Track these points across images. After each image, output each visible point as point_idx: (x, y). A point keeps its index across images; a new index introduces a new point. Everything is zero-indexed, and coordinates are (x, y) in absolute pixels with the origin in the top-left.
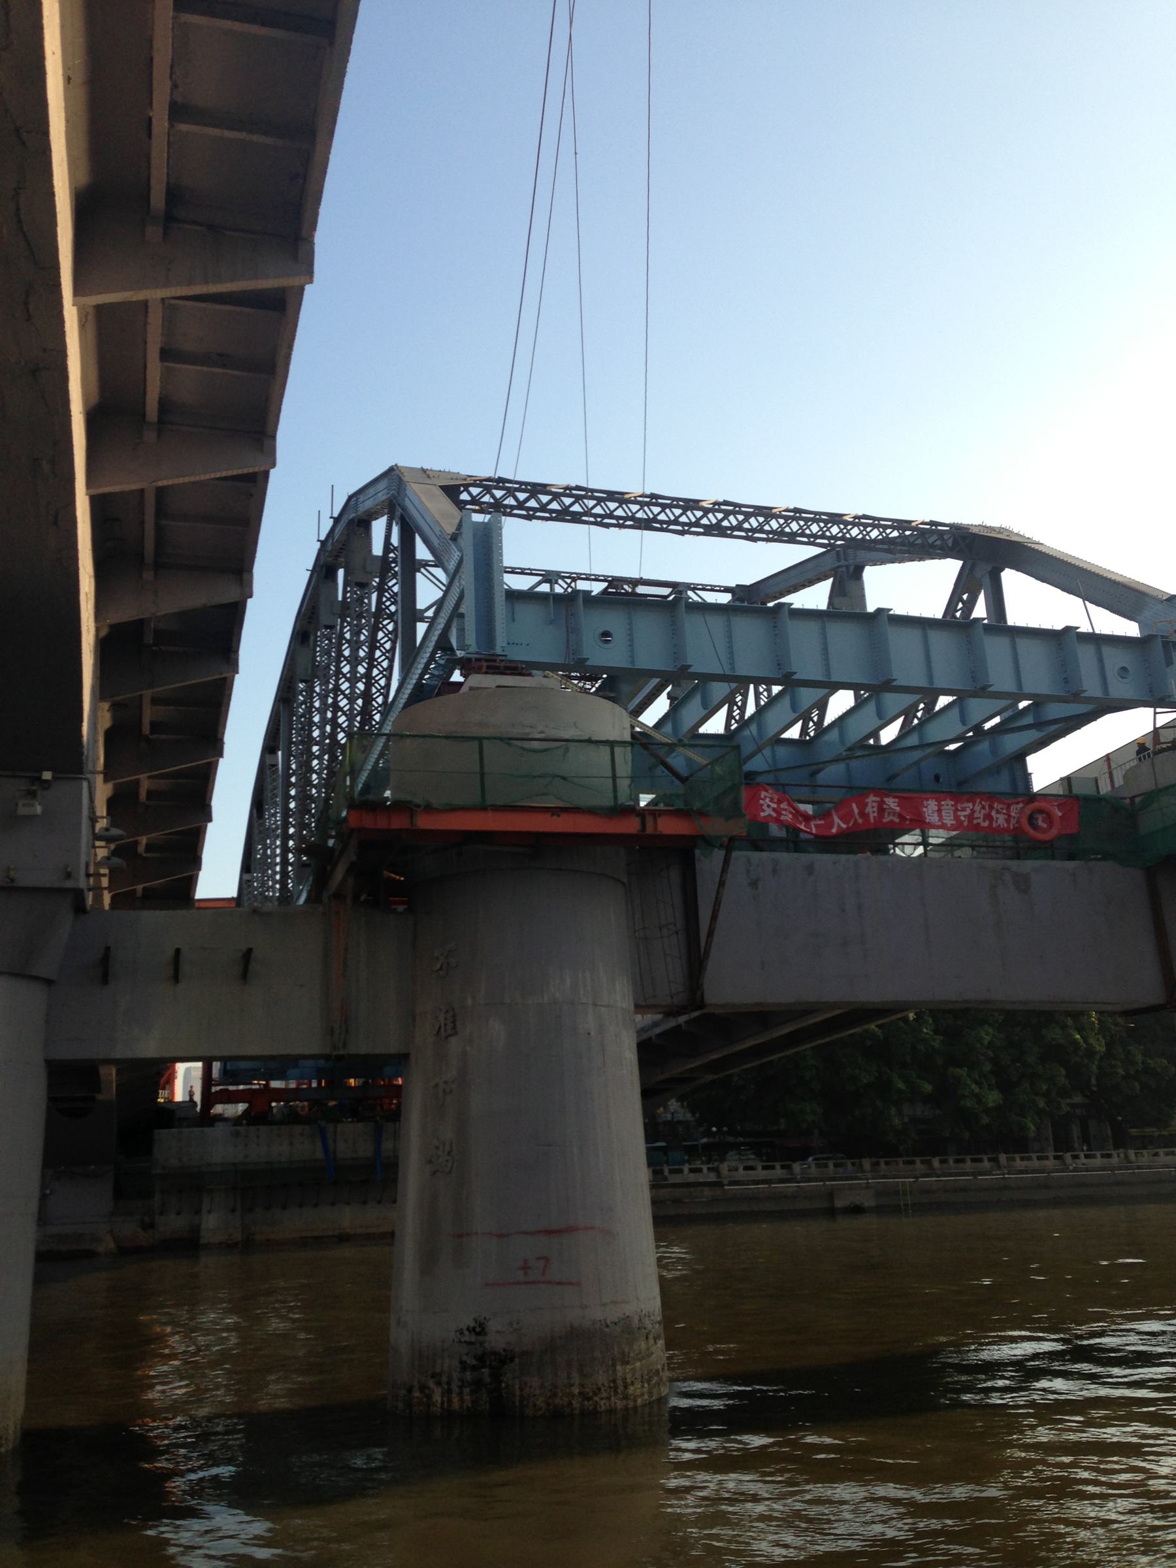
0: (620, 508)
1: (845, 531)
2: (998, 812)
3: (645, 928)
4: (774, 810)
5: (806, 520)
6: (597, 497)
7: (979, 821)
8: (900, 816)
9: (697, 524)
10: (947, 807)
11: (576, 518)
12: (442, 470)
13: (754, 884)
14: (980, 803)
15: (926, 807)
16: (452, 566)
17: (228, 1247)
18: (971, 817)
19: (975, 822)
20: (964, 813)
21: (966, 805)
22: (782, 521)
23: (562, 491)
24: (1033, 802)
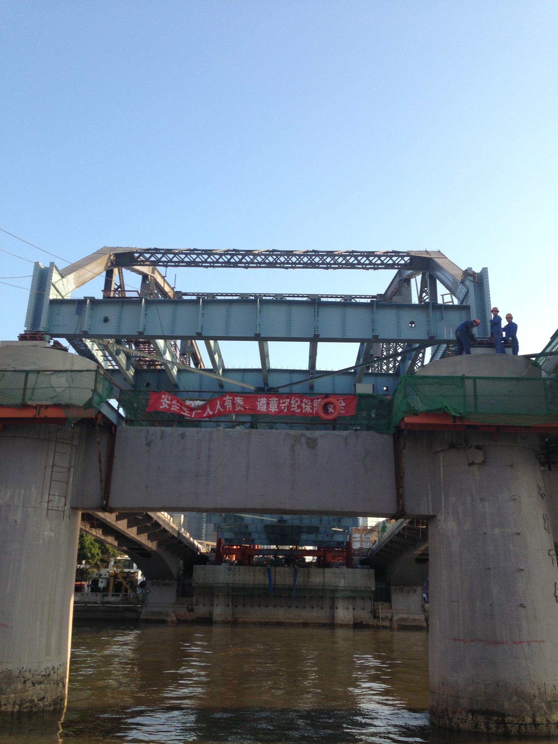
0: (194, 258)
1: (300, 259)
2: (306, 404)
4: (168, 405)
5: (277, 255)
6: (162, 252)
7: (294, 409)
8: (244, 408)
9: (217, 262)
10: (273, 402)
11: (352, 266)
12: (128, 247)
13: (149, 444)
14: (295, 399)
15: (259, 402)
16: (462, 296)
17: (225, 623)
18: (289, 407)
19: (292, 410)
20: (284, 405)
21: (285, 400)
22: (263, 257)
23: (383, 254)
24: (328, 398)
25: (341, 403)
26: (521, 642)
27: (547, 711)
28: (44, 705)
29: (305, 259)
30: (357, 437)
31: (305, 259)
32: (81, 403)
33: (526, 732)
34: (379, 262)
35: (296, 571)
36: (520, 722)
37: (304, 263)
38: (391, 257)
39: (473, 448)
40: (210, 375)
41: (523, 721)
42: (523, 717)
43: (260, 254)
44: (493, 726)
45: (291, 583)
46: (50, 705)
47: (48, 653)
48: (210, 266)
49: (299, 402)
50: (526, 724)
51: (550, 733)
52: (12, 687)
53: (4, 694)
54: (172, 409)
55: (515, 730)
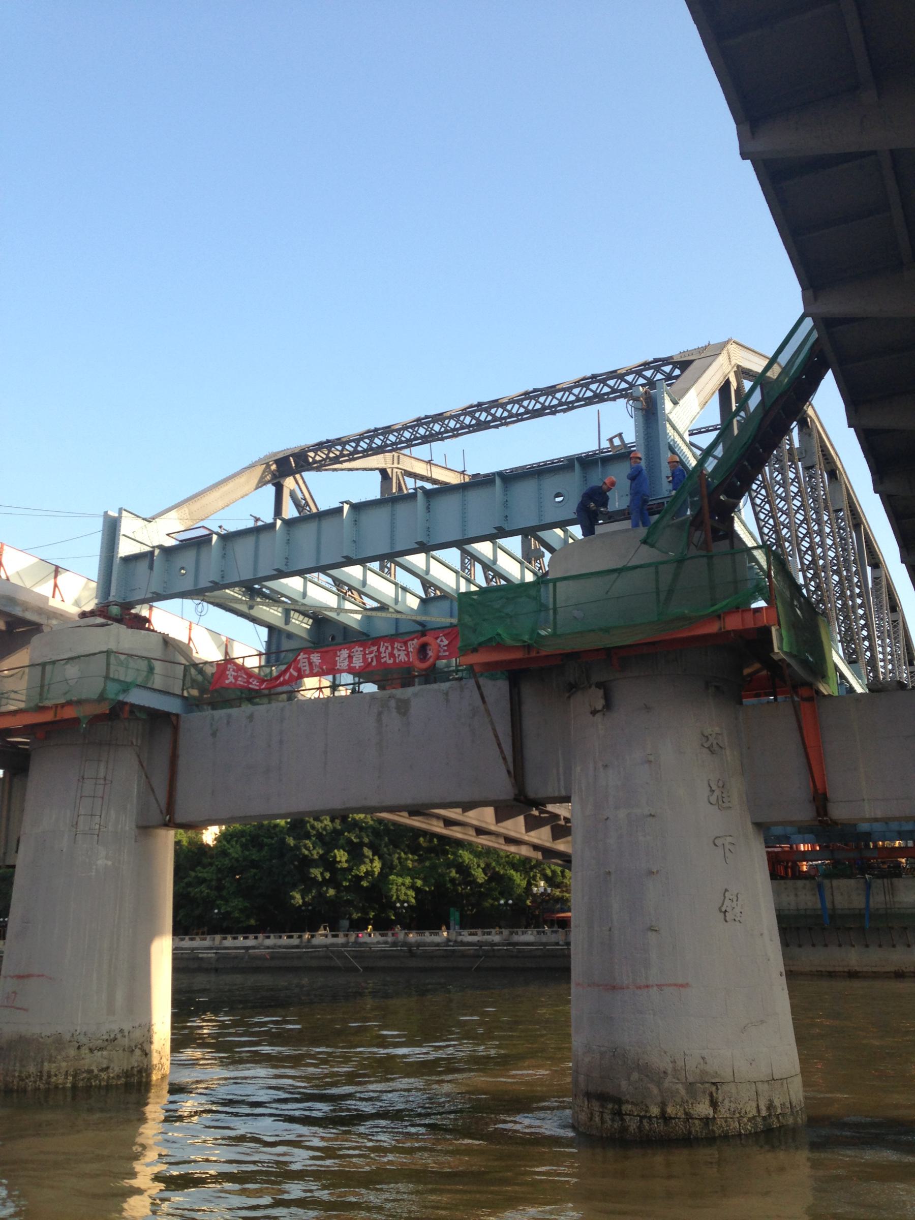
2: (399, 650)
3: (96, 778)
7: (385, 659)
18: (378, 657)
19: (383, 660)
24: (425, 636)
25: (442, 641)
26: (647, 986)
27: (686, 1098)
28: (108, 1077)
29: (422, 431)
30: (462, 689)
31: (422, 431)
32: (95, 697)
33: (651, 1129)
34: (522, 410)
35: (868, 886)
36: (643, 1114)
37: (422, 437)
38: (587, 386)
39: (593, 687)
40: (379, 614)
41: (646, 1112)
42: (647, 1107)
43: (405, 427)
44: (607, 1117)
45: (863, 906)
46: (118, 1077)
47: (111, 1011)
48: (502, 425)
49: (390, 648)
50: (650, 1118)
51: (690, 1133)
52: (63, 1054)
53: (55, 1062)
54: (239, 682)
55: (635, 1126)
